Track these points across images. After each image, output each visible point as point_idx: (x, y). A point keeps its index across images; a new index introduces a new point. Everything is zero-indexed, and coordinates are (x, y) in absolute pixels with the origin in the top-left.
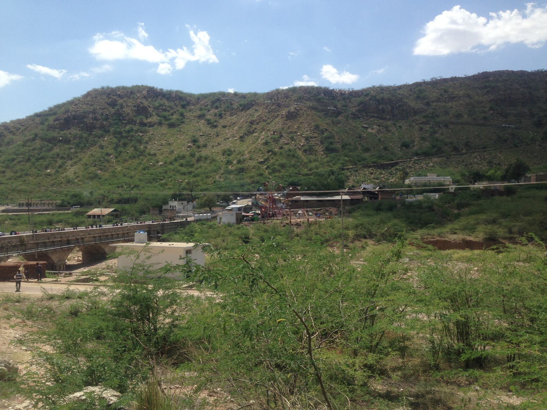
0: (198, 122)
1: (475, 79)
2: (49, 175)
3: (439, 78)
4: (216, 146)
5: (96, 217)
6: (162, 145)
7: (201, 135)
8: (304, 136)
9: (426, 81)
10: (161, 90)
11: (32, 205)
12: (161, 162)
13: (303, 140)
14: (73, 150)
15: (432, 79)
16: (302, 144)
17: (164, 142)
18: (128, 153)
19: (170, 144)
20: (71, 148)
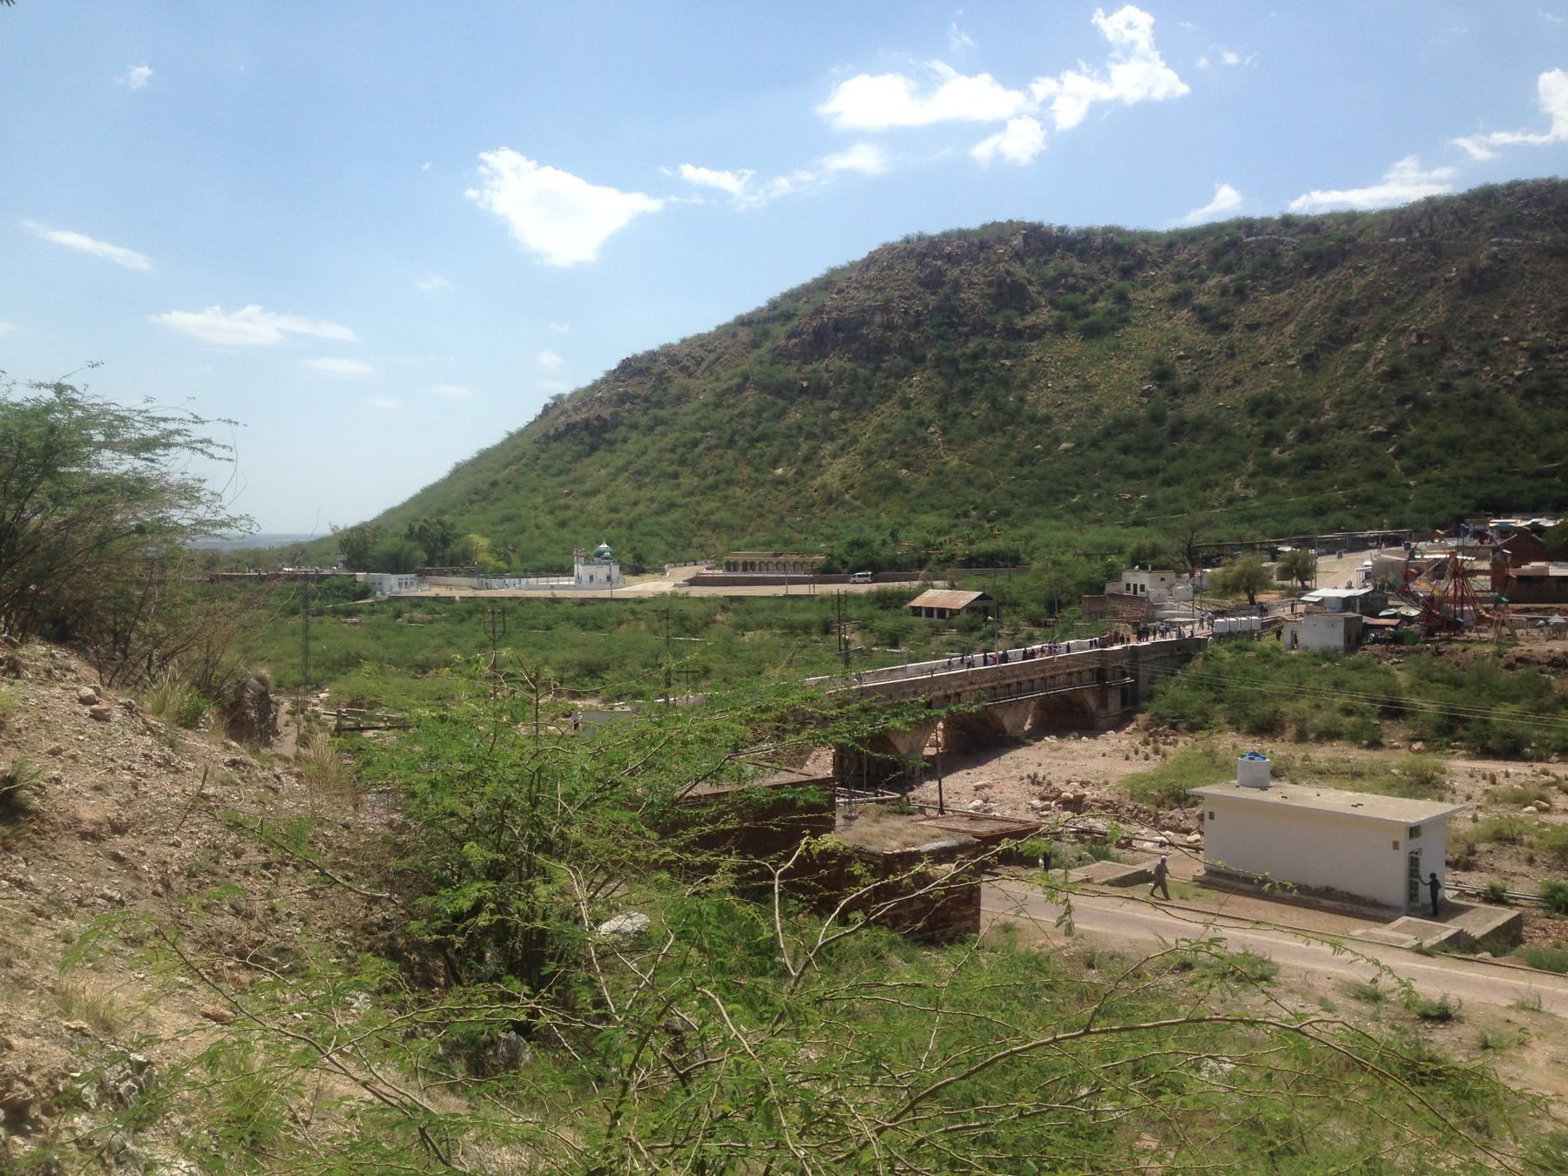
0: (1170, 318)
2: (781, 482)
5: (935, 613)
7: (1181, 358)
8: (1524, 344)
10: (1062, 229)
12: (1067, 441)
14: (835, 415)
18: (974, 417)
19: (1088, 388)
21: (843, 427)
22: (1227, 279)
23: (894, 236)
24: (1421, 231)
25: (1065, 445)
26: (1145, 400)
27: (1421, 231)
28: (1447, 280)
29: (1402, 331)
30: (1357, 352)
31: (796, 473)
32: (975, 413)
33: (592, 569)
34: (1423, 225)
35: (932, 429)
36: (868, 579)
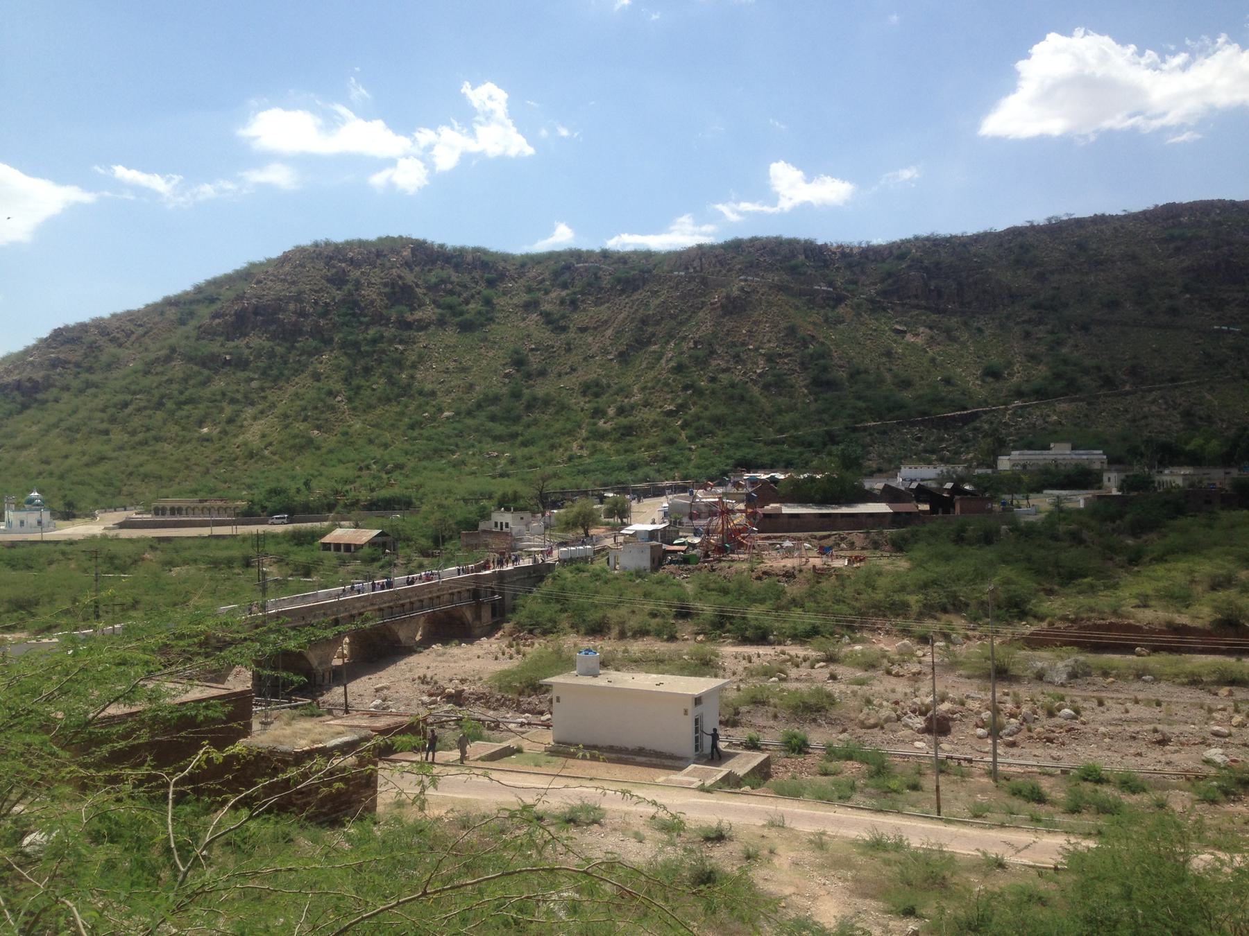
0: (524, 319)
1: (1147, 219)
2: (206, 439)
3: (1065, 218)
4: (567, 374)
6: (447, 371)
7: (532, 350)
8: (762, 351)
9: (1035, 224)
10: (442, 246)
11: (184, 512)
12: (448, 410)
13: (761, 362)
14: (254, 384)
15: (1049, 220)
16: (758, 371)
17: (452, 365)
18: (374, 390)
19: (464, 370)
20: (252, 379)
21: (263, 394)
22: (564, 293)
23: (306, 239)
24: (695, 268)
25: (446, 414)
26: (507, 381)
27: (695, 268)
28: (712, 304)
29: (684, 338)
30: (655, 352)
31: (220, 432)
32: (374, 387)
33: (22, 515)
34: (695, 264)
35: (339, 398)
36: (285, 521)
